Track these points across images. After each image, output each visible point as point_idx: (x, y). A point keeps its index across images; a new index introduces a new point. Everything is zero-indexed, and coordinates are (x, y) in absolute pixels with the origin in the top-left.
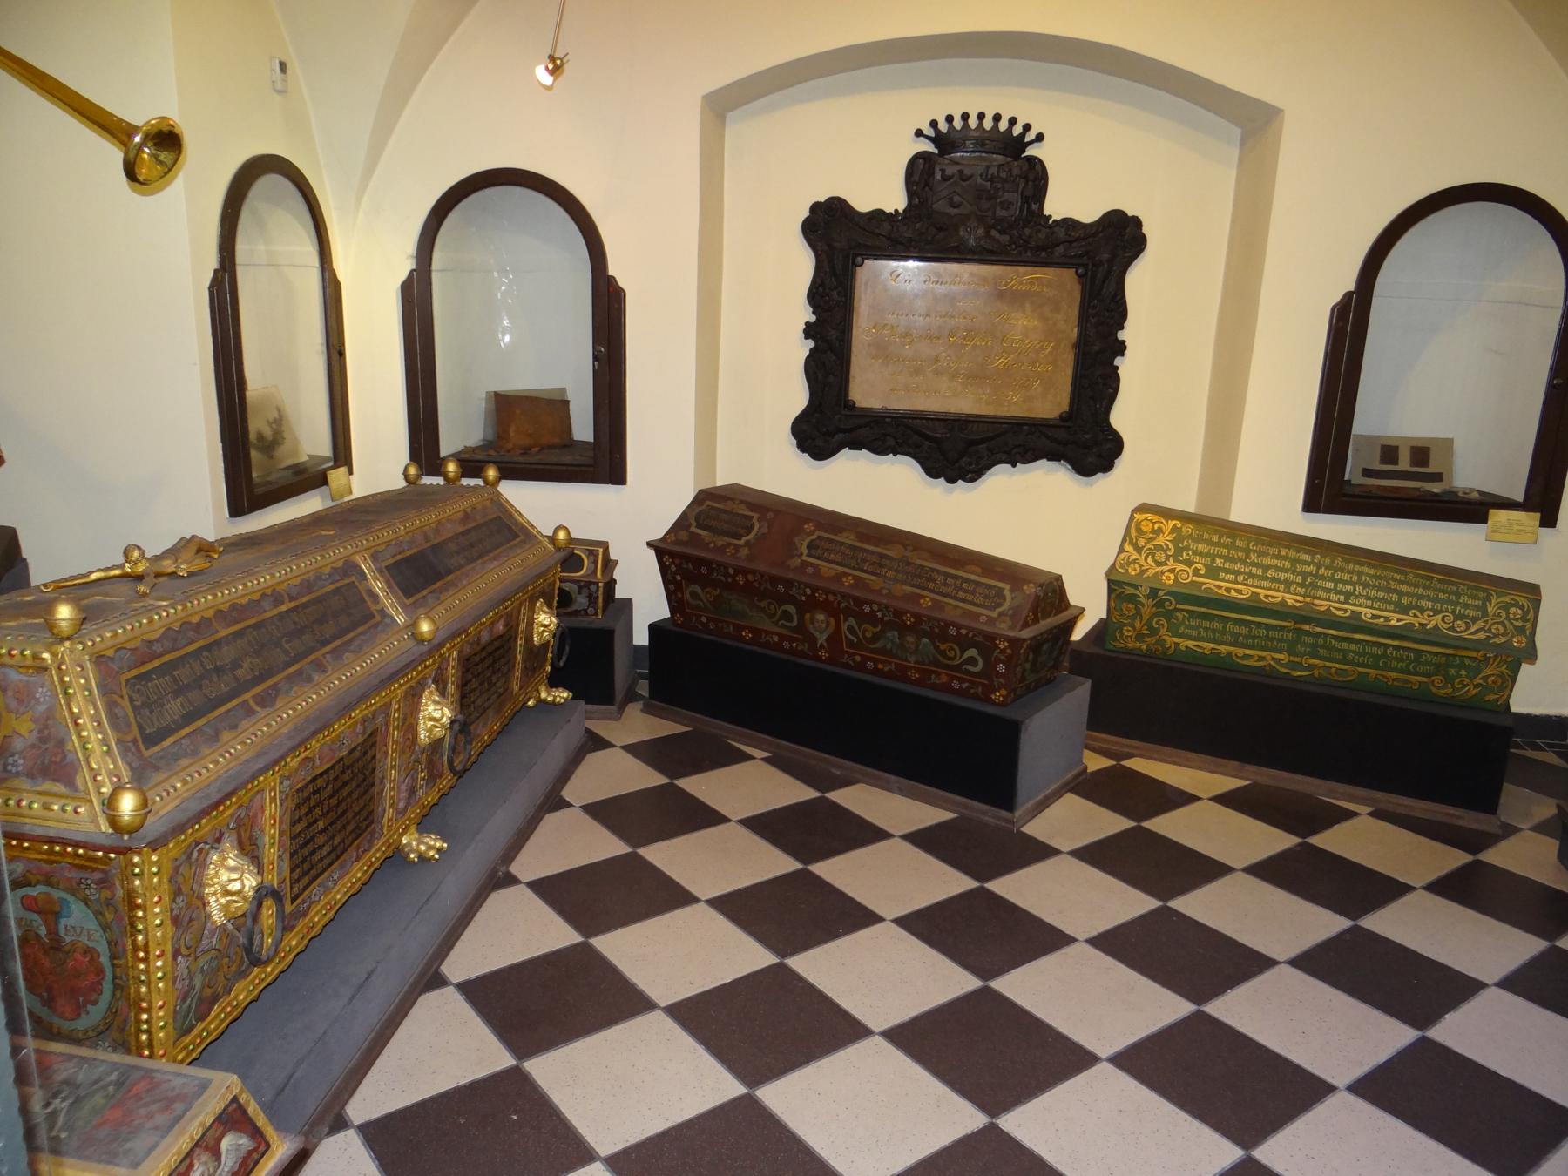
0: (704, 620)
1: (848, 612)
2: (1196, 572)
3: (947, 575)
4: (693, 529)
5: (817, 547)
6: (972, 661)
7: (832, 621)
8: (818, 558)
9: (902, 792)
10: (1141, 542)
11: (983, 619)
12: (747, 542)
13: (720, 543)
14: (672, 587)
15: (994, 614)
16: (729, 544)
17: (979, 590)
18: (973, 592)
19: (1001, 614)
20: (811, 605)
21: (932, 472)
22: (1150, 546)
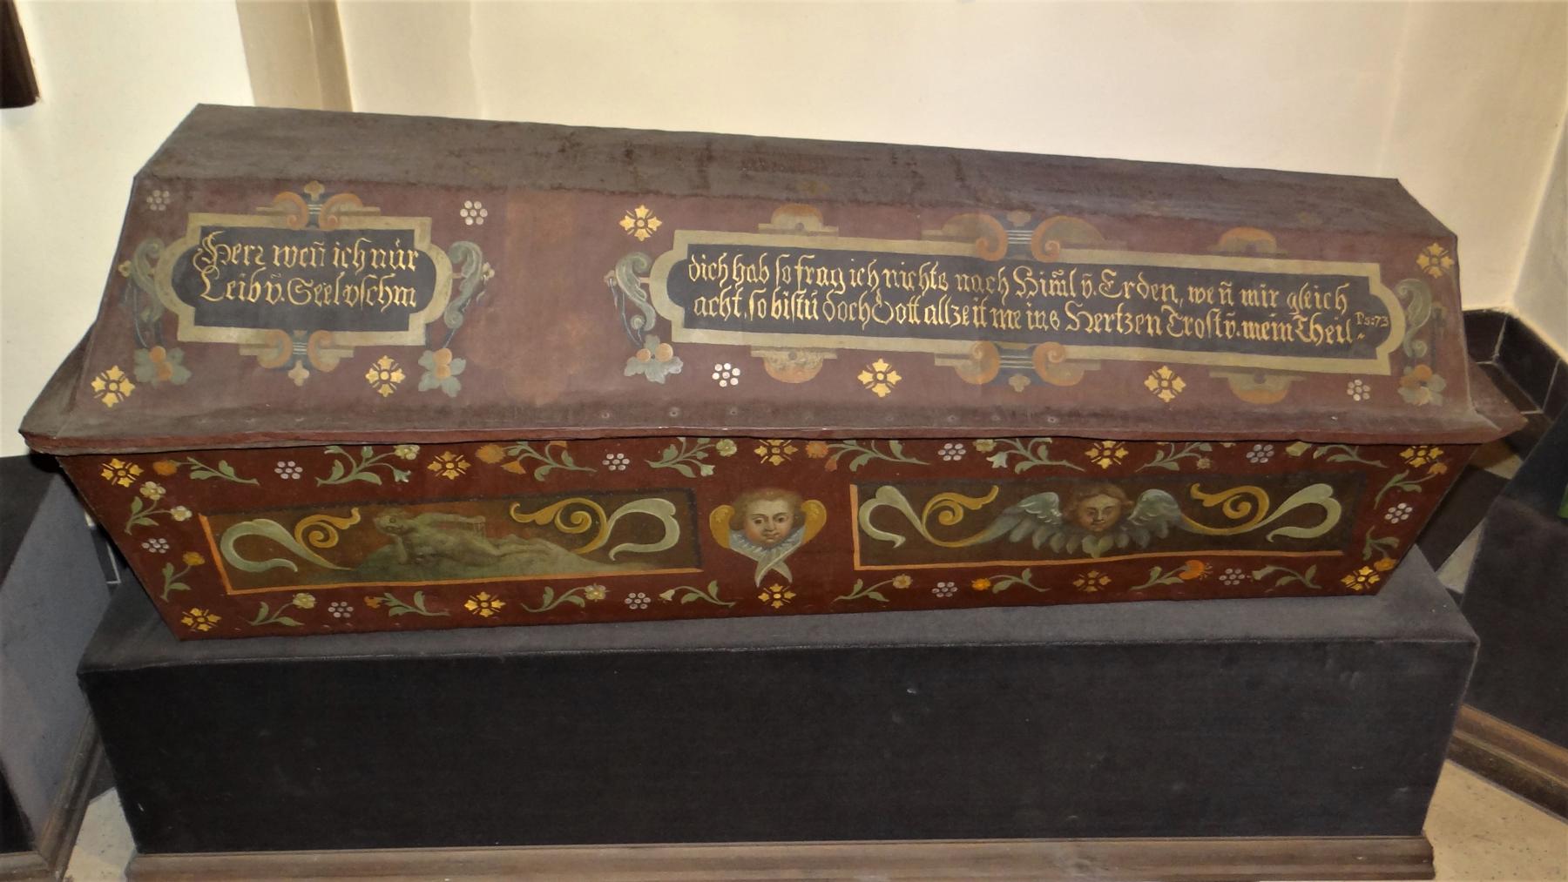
0: (305, 601)
3: (1183, 278)
5: (711, 288)
6: (1313, 514)
7: (816, 511)
11: (1358, 393)
12: (438, 334)
13: (328, 359)
15: (1381, 365)
16: (368, 356)
17: (1296, 301)
18: (1284, 315)
19: (1400, 359)
20: (744, 475)
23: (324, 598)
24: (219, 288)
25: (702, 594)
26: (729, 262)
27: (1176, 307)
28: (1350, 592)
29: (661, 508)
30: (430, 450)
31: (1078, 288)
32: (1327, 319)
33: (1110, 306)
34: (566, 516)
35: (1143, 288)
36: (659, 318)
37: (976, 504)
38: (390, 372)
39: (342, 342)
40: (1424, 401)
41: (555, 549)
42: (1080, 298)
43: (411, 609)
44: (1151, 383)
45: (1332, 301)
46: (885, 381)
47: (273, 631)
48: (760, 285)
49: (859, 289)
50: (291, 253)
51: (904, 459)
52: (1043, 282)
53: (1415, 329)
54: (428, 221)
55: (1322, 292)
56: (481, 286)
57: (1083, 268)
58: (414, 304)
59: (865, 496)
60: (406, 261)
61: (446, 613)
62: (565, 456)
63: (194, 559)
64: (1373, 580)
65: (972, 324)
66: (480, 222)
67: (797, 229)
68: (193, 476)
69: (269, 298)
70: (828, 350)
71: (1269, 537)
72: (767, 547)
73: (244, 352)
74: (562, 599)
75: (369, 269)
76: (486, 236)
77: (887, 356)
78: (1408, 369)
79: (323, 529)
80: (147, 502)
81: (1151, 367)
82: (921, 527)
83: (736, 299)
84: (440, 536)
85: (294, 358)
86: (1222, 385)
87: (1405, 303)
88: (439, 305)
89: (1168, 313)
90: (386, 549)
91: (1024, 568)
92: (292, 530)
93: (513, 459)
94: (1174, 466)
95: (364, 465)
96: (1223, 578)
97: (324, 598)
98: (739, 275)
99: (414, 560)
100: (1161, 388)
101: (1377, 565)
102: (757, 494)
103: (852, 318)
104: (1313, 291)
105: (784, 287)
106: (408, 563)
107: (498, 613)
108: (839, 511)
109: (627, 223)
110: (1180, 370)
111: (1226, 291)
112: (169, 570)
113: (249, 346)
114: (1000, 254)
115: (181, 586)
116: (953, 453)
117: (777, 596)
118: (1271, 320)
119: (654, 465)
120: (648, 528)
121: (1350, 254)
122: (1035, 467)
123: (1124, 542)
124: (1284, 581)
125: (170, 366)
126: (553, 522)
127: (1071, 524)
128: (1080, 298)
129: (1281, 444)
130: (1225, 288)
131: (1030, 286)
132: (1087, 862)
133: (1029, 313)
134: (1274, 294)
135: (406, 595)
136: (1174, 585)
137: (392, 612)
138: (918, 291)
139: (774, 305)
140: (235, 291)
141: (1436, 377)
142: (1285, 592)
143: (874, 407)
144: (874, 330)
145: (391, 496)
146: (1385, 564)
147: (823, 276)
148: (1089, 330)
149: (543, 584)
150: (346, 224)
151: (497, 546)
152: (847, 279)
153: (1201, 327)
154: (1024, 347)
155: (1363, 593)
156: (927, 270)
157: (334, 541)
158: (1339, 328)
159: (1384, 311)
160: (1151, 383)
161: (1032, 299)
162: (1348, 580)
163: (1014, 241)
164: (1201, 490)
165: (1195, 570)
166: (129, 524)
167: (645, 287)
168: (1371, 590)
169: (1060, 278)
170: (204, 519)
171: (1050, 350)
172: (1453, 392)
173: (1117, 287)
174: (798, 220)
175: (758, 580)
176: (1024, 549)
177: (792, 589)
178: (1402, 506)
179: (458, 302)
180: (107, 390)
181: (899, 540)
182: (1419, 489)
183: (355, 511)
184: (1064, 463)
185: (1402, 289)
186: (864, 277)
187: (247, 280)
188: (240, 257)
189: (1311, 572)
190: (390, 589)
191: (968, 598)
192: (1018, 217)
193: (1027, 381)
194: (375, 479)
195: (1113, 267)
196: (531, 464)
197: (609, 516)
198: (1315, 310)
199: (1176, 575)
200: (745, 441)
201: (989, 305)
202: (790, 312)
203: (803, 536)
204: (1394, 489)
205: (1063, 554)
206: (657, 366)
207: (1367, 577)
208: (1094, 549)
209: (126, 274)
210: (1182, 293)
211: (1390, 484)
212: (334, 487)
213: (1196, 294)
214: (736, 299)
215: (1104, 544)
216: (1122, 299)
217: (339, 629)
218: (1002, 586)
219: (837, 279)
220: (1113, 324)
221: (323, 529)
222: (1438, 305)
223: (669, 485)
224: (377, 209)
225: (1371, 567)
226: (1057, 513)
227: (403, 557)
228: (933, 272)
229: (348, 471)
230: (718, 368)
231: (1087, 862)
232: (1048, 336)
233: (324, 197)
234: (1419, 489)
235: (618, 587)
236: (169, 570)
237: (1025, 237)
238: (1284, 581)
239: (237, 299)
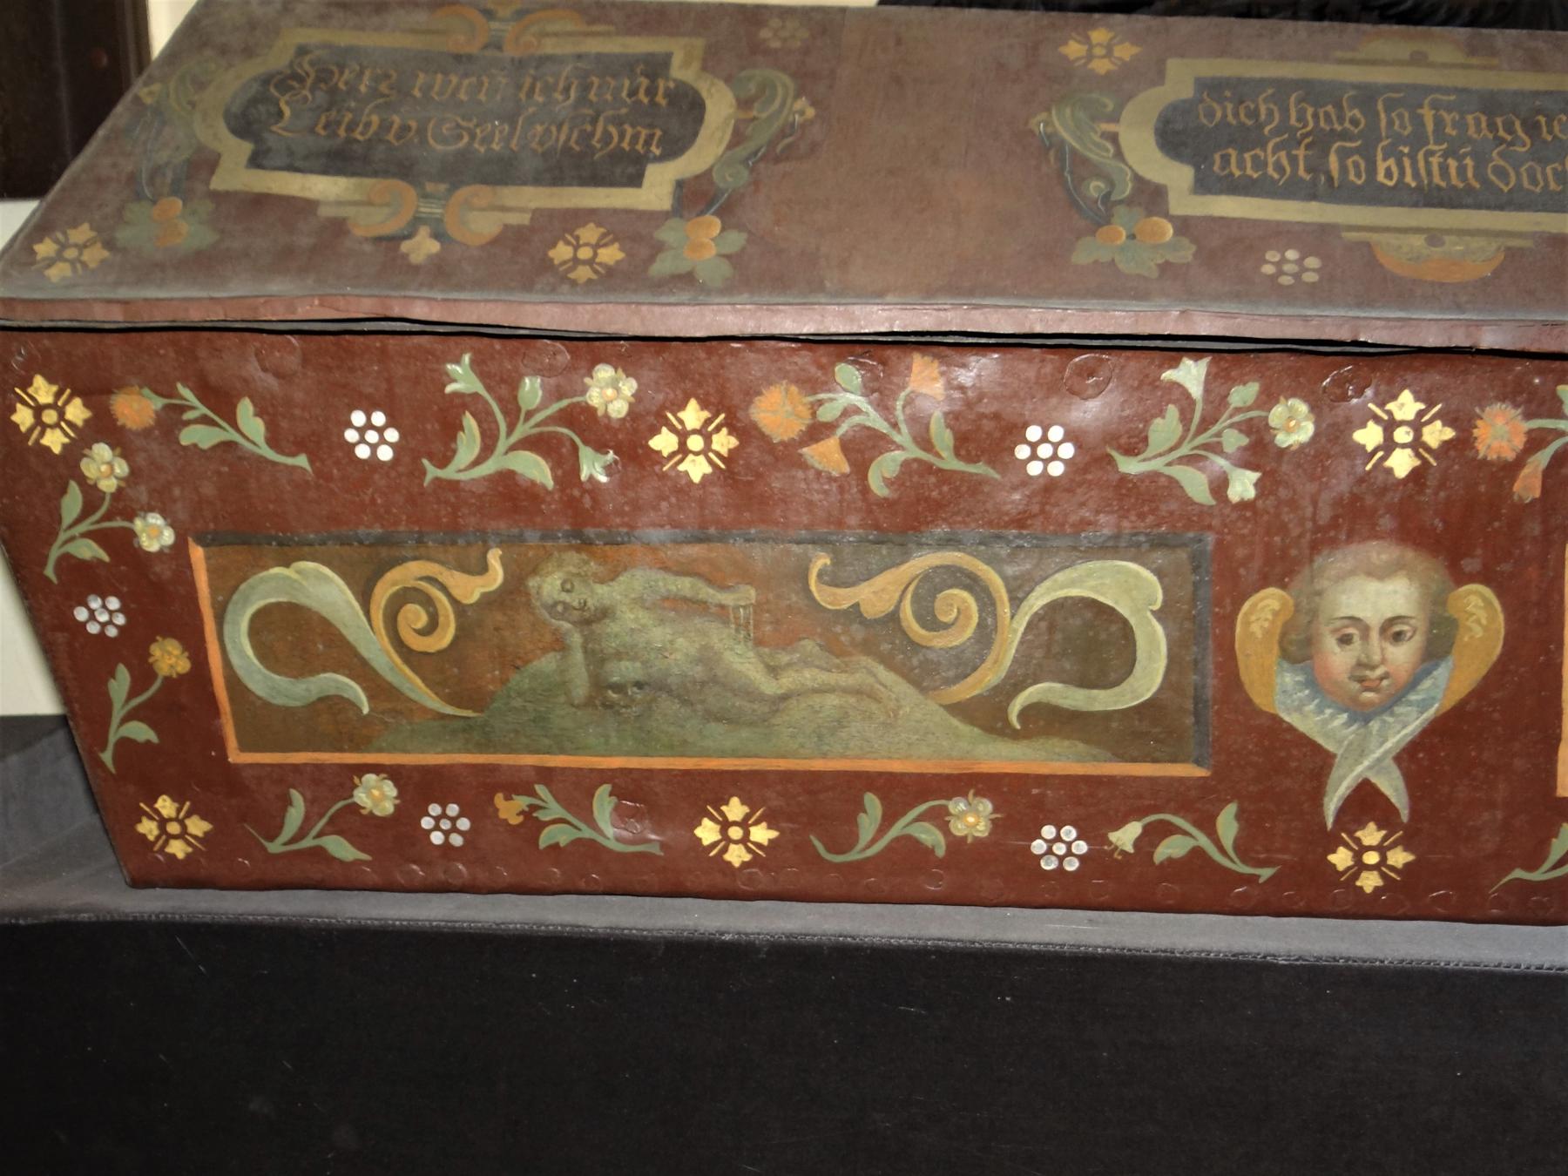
0: (377, 796)
7: (1480, 611)
12: (694, 197)
23: (420, 787)
25: (1203, 841)
29: (1130, 587)
36: (1138, 179)
38: (596, 247)
43: (587, 833)
63: (169, 658)
68: (188, 436)
70: (1520, 235)
72: (1361, 715)
84: (659, 635)
90: (547, 663)
92: (365, 598)
95: (522, 430)
97: (420, 787)
99: (606, 697)
105: (1398, 140)
106: (589, 702)
107: (765, 858)
112: (120, 684)
113: (339, 203)
115: (141, 732)
117: (1371, 858)
126: (893, 617)
135: (576, 790)
139: (1381, 167)
149: (854, 785)
166: (55, 553)
167: (1114, 138)
170: (197, 553)
179: (741, 152)
183: (494, 557)
190: (546, 775)
194: (536, 469)
197: (1016, 602)
202: (1416, 175)
203: (1446, 687)
209: (148, 101)
212: (453, 485)
221: (428, 602)
229: (487, 449)
235: (1022, 803)
236: (120, 684)
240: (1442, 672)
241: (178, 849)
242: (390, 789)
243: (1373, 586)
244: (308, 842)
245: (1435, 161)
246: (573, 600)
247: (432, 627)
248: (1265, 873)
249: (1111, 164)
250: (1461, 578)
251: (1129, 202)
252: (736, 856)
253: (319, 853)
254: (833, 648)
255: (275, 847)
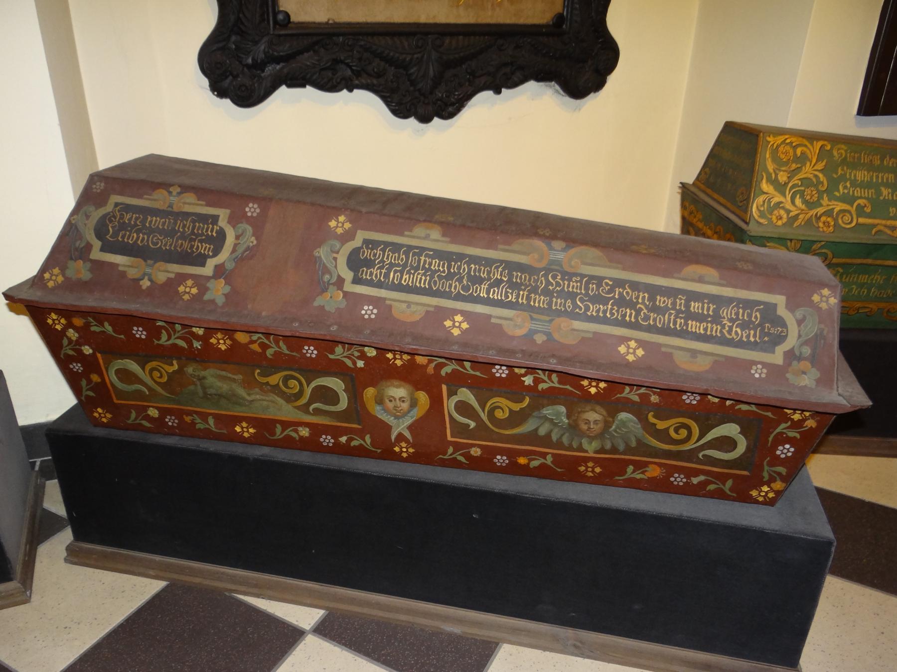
0: (153, 413)
1: (457, 381)
2: (860, 211)
3: (654, 291)
4: (97, 254)
5: (369, 263)
6: (727, 443)
7: (423, 397)
8: (379, 285)
9: (580, 650)
10: (782, 177)
11: (758, 373)
12: (219, 271)
13: (161, 278)
14: (77, 367)
16: (182, 278)
17: (726, 313)
18: (716, 319)
19: (790, 355)
20: (380, 371)
21: (400, 110)
22: (795, 181)
23: (164, 412)
24: (115, 234)
25: (362, 442)
26: (383, 250)
27: (647, 307)
28: (757, 502)
29: (335, 383)
30: (210, 331)
31: (587, 289)
32: (744, 326)
33: (605, 301)
34: (286, 379)
35: (627, 293)
36: (339, 276)
37: (516, 407)
38: (191, 288)
39: (170, 269)
40: (802, 384)
41: (280, 401)
42: (587, 294)
43: (207, 426)
44: (622, 349)
45: (750, 316)
46: (459, 327)
47: (137, 428)
48: (398, 265)
49: (455, 274)
50: (156, 221)
51: (472, 372)
52: (566, 283)
53: (803, 339)
54: (228, 211)
55: (744, 309)
56: (248, 249)
57: (592, 277)
58: (211, 254)
59: (451, 393)
60: (212, 231)
61: (225, 432)
62: (281, 343)
64: (771, 495)
65: (517, 301)
66: (255, 215)
67: (428, 237)
69: (139, 242)
71: (700, 455)
73: (121, 268)
74: (285, 433)
75: (193, 233)
76: (258, 224)
77: (462, 313)
78: (795, 363)
79: (159, 371)
80: (70, 341)
81: (625, 340)
82: (484, 417)
83: (383, 271)
84: (219, 384)
85: (145, 274)
86: (669, 356)
87: (800, 322)
88: (223, 256)
89: (641, 309)
90: (192, 387)
91: (548, 453)
92: (143, 369)
93: (255, 342)
94: (636, 399)
95: (177, 335)
96: (672, 479)
97: (164, 412)
98: (388, 258)
100: (628, 353)
101: (772, 485)
102: (389, 384)
103: (447, 289)
104: (739, 308)
105: (412, 267)
107: (253, 436)
108: (436, 402)
109: (333, 224)
110: (641, 343)
111: (681, 301)
112: (84, 383)
113: (124, 266)
114: (543, 264)
115: (91, 394)
116: (501, 372)
118: (708, 322)
119: (331, 357)
120: (329, 396)
121: (769, 290)
122: (550, 388)
123: (608, 446)
124: (711, 487)
125: (83, 271)
127: (573, 427)
128: (587, 294)
129: (704, 395)
130: (681, 299)
131: (558, 284)
132: (578, 644)
133: (554, 300)
134: (712, 307)
135: (204, 417)
136: (641, 479)
137: (198, 426)
138: (489, 279)
139: (404, 277)
140: (123, 237)
141: (814, 370)
142: (712, 495)
143: (448, 339)
144: (458, 297)
145: (190, 356)
146: (778, 485)
147: (435, 264)
148: (589, 314)
150: (188, 209)
151: (249, 395)
152: (449, 267)
153: (660, 321)
154: (547, 318)
155: (764, 503)
156: (497, 268)
157: (165, 379)
158: (752, 332)
159: (784, 325)
160: (622, 349)
161: (557, 292)
162: (754, 493)
163: (552, 257)
164: (654, 416)
165: (653, 472)
166: (63, 352)
167: (335, 259)
168: (771, 503)
169: (577, 282)
170: (99, 355)
171: (564, 323)
172: (825, 381)
173: (612, 291)
174: (428, 232)
175: (393, 437)
176: (546, 441)
177: (413, 447)
178: (787, 446)
179: (234, 256)
180: (51, 279)
181: (473, 424)
182: (798, 436)
183: (175, 362)
184: (568, 387)
185: (799, 313)
186: (459, 268)
187: (130, 231)
188: (130, 219)
189: (729, 483)
190: (196, 413)
191: (513, 469)
192: (558, 244)
193: (545, 338)
195: (610, 279)
196: (264, 347)
198: (737, 319)
199: (643, 473)
200: (381, 350)
201: (530, 292)
204: (781, 434)
205: (570, 448)
206: (331, 301)
207: (767, 493)
208: (590, 448)
210: (652, 299)
211: (778, 430)
212: (162, 346)
213: (661, 301)
214: (383, 271)
215: (595, 445)
216: (613, 297)
217: (171, 432)
218: (535, 464)
219: (443, 267)
220: (605, 312)
221: (159, 371)
222: (822, 326)
223: (338, 369)
224: (204, 203)
225: (769, 486)
226: (566, 420)
227: (201, 394)
228: (500, 269)
229: (169, 338)
230: (366, 308)
231: (578, 644)
232: (559, 313)
233: (179, 194)
234: (798, 436)
237: (561, 256)
238: (711, 487)
239: (123, 241)
240: (415, 410)
241: (104, 420)
242: (157, 412)
243: (395, 390)
244: (138, 421)
245: (419, 276)
246: (196, 374)
247: (161, 377)
248: (379, 451)
249: (332, 269)
250: (418, 389)
251: (333, 284)
252: (246, 435)
253: (141, 425)
254: (262, 390)
255: (129, 422)
